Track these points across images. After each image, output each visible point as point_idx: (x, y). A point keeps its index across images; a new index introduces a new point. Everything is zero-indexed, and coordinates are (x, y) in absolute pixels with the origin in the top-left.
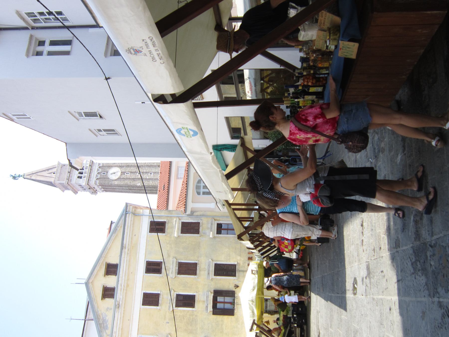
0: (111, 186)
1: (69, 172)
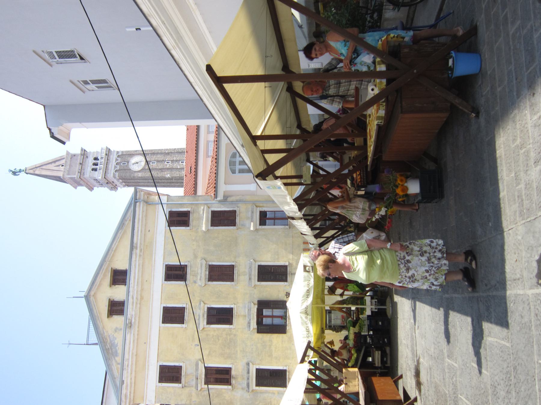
0: (134, 179)
1: (81, 164)
